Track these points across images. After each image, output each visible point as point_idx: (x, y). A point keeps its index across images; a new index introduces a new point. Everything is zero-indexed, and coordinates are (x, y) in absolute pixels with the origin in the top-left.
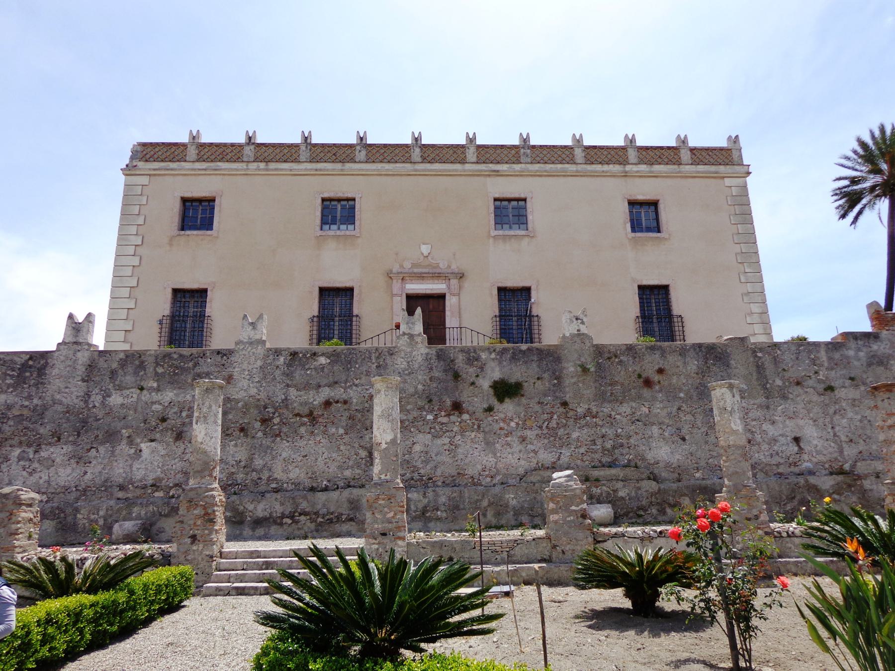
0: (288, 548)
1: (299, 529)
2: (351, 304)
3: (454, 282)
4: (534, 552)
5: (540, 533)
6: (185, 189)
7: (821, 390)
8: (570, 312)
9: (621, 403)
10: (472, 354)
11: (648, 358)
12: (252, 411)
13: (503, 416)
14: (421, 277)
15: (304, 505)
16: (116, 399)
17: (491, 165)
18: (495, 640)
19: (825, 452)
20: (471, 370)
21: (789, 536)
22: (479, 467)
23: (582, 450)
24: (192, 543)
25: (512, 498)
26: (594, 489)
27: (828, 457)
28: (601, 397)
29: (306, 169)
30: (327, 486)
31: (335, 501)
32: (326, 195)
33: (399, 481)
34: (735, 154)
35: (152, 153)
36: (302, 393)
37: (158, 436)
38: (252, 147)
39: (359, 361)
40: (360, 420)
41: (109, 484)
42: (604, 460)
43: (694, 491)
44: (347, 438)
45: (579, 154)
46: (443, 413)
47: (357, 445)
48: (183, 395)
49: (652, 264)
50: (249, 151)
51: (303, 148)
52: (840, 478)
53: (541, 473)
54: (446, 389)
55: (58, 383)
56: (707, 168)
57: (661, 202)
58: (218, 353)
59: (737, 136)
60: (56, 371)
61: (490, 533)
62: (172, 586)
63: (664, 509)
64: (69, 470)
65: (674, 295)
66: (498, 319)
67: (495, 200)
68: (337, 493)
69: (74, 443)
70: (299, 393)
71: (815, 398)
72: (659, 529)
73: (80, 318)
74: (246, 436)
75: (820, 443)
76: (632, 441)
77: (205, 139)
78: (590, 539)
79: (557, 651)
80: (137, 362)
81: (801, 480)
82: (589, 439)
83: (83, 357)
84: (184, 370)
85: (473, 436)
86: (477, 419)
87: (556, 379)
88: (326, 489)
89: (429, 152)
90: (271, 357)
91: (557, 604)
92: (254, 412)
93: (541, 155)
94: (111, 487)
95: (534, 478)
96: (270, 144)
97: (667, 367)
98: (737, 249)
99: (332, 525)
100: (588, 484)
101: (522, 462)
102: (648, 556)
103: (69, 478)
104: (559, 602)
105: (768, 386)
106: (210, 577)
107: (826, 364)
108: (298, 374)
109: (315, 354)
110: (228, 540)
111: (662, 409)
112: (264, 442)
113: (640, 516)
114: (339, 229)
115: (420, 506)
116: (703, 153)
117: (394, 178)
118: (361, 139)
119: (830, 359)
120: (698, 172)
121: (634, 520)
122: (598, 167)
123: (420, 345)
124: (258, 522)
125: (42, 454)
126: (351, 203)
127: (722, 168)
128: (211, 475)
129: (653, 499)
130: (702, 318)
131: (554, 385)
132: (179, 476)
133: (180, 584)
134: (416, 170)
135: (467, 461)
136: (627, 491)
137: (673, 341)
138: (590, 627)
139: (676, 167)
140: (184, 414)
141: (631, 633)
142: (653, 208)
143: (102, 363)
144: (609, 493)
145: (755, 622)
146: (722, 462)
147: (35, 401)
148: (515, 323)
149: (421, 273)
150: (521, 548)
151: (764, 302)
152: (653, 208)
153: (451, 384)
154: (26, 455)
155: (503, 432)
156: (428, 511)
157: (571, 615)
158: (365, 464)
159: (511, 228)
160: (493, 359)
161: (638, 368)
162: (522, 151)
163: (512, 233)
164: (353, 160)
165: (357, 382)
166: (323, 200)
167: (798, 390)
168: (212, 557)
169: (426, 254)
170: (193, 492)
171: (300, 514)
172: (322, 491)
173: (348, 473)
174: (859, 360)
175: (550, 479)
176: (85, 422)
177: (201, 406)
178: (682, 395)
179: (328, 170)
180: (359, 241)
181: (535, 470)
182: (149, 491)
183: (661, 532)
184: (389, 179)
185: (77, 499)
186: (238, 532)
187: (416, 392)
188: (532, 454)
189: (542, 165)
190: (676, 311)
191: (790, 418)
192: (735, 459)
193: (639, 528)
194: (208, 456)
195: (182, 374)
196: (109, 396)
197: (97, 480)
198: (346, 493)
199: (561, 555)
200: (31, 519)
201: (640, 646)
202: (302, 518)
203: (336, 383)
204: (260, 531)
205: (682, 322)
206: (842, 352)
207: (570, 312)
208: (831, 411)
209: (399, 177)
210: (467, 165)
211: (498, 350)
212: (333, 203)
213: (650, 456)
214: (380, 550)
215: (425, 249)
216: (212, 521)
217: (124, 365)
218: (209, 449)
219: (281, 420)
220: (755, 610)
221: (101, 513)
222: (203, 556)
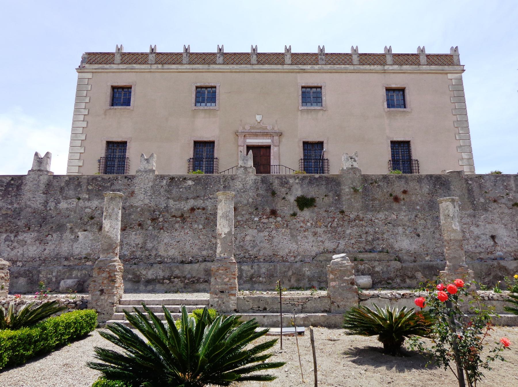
0: (162, 299)
1: (174, 286)
2: (213, 151)
3: (276, 138)
4: (319, 305)
5: (324, 293)
6: (114, 80)
7: (511, 206)
8: (347, 154)
9: (378, 212)
10: (283, 180)
11: (397, 184)
12: (146, 213)
13: (302, 219)
14: (256, 135)
15: (177, 272)
16: (63, 205)
17: (300, 66)
18: (286, 370)
19: (512, 245)
20: (283, 190)
21: (489, 299)
22: (287, 251)
23: (353, 241)
24: (101, 294)
25: (307, 271)
26: (360, 266)
27: (513, 250)
28: (366, 208)
29: (186, 69)
30: (191, 261)
31: (195, 270)
32: (198, 85)
33: (233, 258)
34: (455, 59)
35: (94, 59)
36: (177, 203)
37: (88, 228)
38: (154, 55)
39: (212, 184)
40: (211, 221)
41: (59, 257)
42: (367, 248)
43: (424, 268)
44: (204, 231)
45: (355, 58)
46: (265, 217)
47: (210, 236)
50: (152, 57)
51: (185, 55)
53: (326, 255)
54: (267, 202)
55: (29, 195)
57: (406, 89)
60: (28, 187)
61: (292, 292)
62: (80, 323)
63: (405, 279)
64: (35, 248)
65: (413, 147)
66: (303, 161)
67: (303, 87)
68: (198, 265)
69: (38, 231)
71: (506, 211)
72: (402, 292)
73: (42, 155)
74: (142, 228)
75: (508, 240)
76: (385, 236)
78: (356, 299)
79: (329, 382)
80: (76, 183)
81: (495, 263)
83: (44, 179)
85: (283, 231)
86: (286, 221)
88: (191, 262)
89: (261, 58)
91: (333, 342)
92: (147, 214)
93: (331, 60)
94: (60, 258)
95: (321, 258)
96: (164, 53)
97: (409, 190)
98: (455, 118)
99: (194, 284)
100: (356, 263)
101: (314, 248)
102: (396, 314)
103: (35, 252)
104: (334, 340)
105: (475, 202)
106: (111, 316)
107: (514, 189)
109: (185, 179)
110: (125, 292)
111: (405, 216)
113: (389, 283)
114: (206, 105)
115: (249, 274)
116: (435, 58)
117: (240, 73)
118: (220, 50)
122: (367, 67)
123: (251, 174)
124: (149, 282)
125: (19, 238)
126: (213, 89)
127: (446, 67)
128: (113, 252)
129: (398, 273)
130: (430, 160)
131: (336, 200)
133: (87, 321)
134: (253, 69)
135: (279, 247)
136: (381, 267)
137: (411, 173)
138: (354, 362)
139: (417, 66)
141: (383, 368)
142: (401, 93)
143: (55, 183)
144: (369, 269)
145: (480, 369)
146: (445, 250)
147: (15, 205)
148: (313, 164)
149: (256, 133)
150: (311, 303)
151: (471, 152)
152: (401, 93)
153: (270, 198)
154: (9, 238)
155: (302, 229)
156: (254, 278)
157: (341, 352)
159: (312, 105)
160: (297, 183)
161: (390, 190)
162: (320, 57)
163: (312, 108)
164: (215, 63)
165: (211, 196)
166: (197, 87)
167: (495, 205)
168: (113, 304)
169: (259, 121)
170: (102, 263)
171: (175, 278)
172: (188, 263)
173: (204, 253)
175: (331, 259)
176: (44, 219)
177: (108, 208)
178: (418, 207)
179: (200, 69)
180: (218, 112)
181: (322, 253)
182: (83, 261)
183: (403, 295)
185: (40, 265)
186: (136, 288)
187: (248, 203)
188: (321, 243)
189: (332, 66)
190: (414, 157)
191: (489, 223)
192: (455, 248)
193: (389, 291)
194: (112, 240)
195: (103, 190)
196: (59, 203)
197: (52, 254)
198: (203, 265)
199: (337, 308)
200: (3, 277)
201: (390, 380)
202: (176, 280)
203: (198, 197)
204: (150, 287)
205: (418, 164)
207: (347, 154)
209: (243, 74)
210: (285, 66)
211: (300, 177)
212: (203, 89)
213: (396, 246)
214: (220, 302)
215: (259, 118)
216: (113, 281)
218: (112, 236)
219: (164, 219)
220: (481, 361)
221: (54, 274)
222: (108, 303)
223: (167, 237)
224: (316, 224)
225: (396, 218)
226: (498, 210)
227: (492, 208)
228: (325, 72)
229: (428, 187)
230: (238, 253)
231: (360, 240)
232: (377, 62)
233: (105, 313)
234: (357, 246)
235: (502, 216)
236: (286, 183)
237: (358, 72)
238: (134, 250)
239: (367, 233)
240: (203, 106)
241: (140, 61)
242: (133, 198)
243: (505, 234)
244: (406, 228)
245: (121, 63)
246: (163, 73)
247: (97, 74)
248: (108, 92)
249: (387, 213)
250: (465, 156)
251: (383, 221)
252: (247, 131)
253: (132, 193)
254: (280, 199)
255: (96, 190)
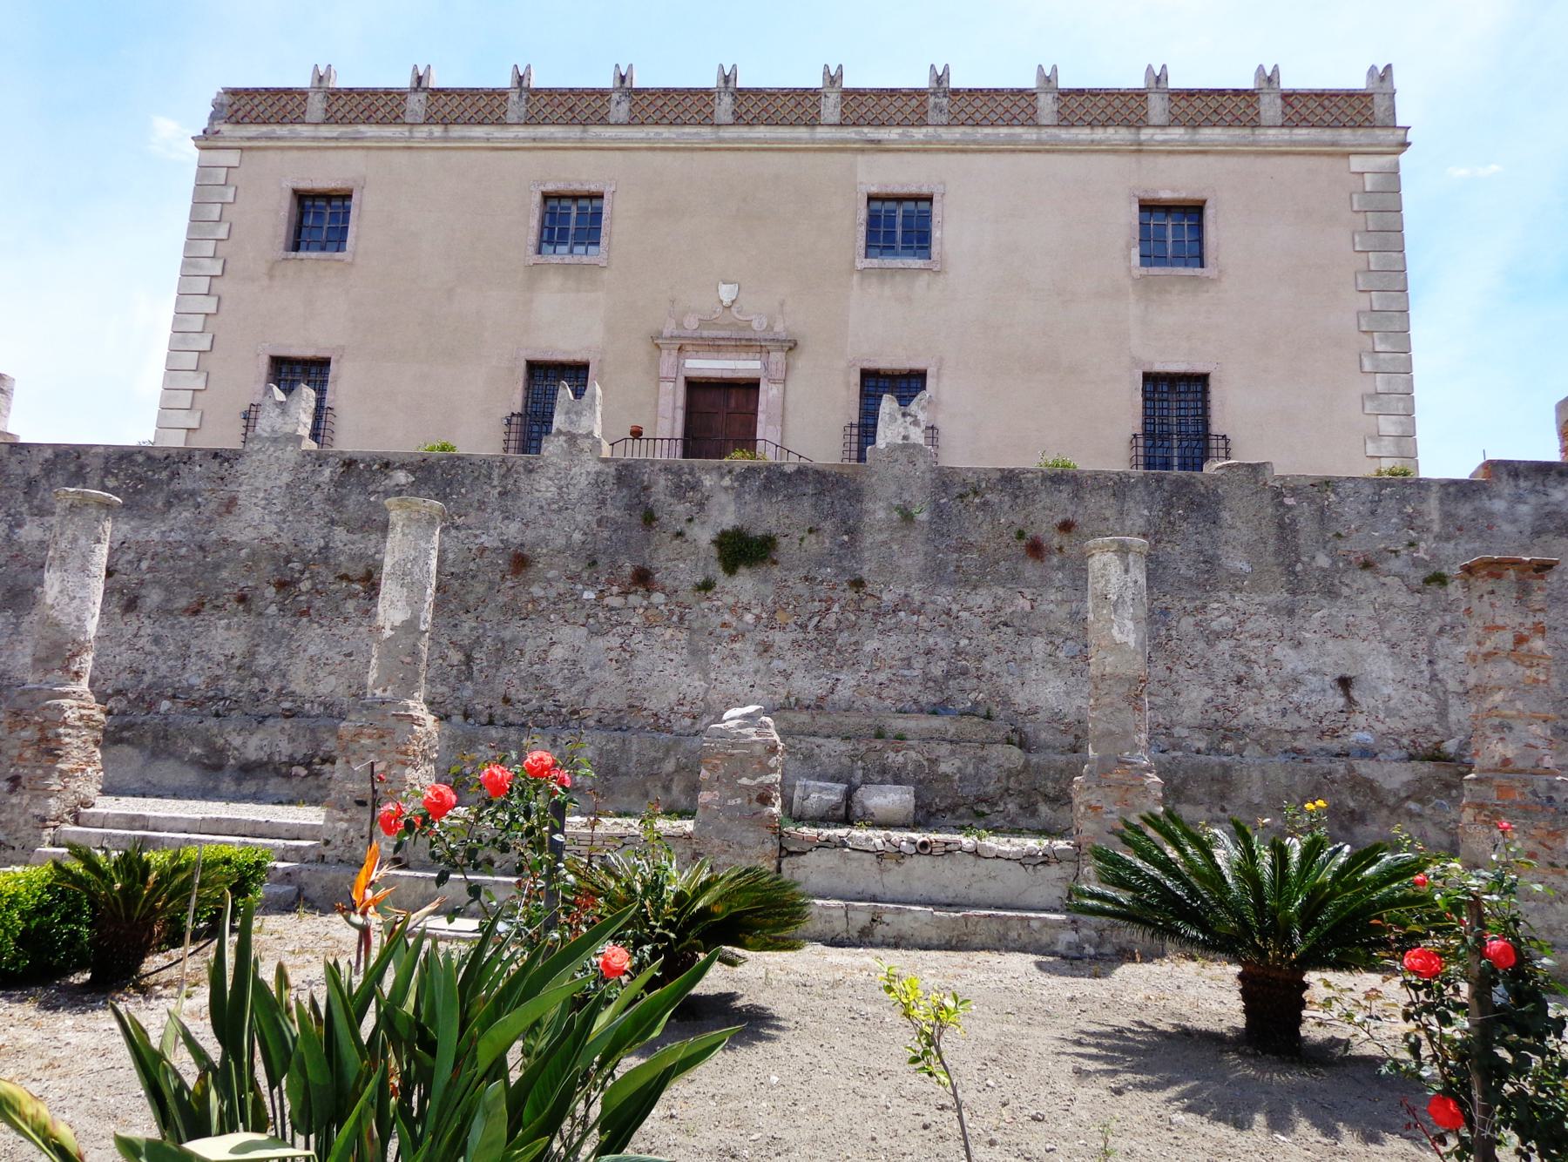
0: (199, 816)
3: (777, 357)
6: (302, 175)
7: (1417, 582)
9: (975, 588)
10: (685, 477)
11: (1044, 499)
12: (262, 565)
13: (730, 600)
14: (715, 346)
17: (866, 130)
19: (1406, 713)
20: (680, 508)
22: (673, 697)
23: (882, 677)
24: (11, 791)
26: (892, 755)
27: (1410, 726)
28: (935, 573)
29: (516, 138)
32: (550, 187)
34: (1380, 104)
35: (248, 108)
38: (422, 96)
39: (467, 482)
42: (923, 700)
45: (1046, 104)
46: (615, 589)
47: (444, 641)
48: (145, 531)
49: (1177, 328)
50: (416, 104)
51: (514, 97)
52: (1426, 768)
53: (789, 715)
56: (1314, 133)
58: (216, 455)
59: (1389, 67)
66: (855, 431)
67: (871, 198)
70: (351, 536)
71: (1402, 598)
72: (919, 837)
74: (248, 611)
77: (340, 82)
80: (72, 467)
81: (1340, 767)
82: (899, 655)
84: (153, 485)
85: (667, 636)
86: (678, 605)
87: (846, 533)
90: (309, 468)
92: (267, 567)
93: (970, 110)
96: (454, 90)
98: (1363, 302)
105: (1299, 567)
107: (1436, 528)
108: (354, 500)
109: (387, 465)
111: (1059, 604)
112: (278, 624)
113: (982, 815)
114: (571, 251)
116: (1312, 104)
118: (623, 79)
119: (1447, 516)
120: (1294, 143)
121: (966, 822)
122: (1083, 134)
123: (585, 457)
124: (248, 770)
127: (1346, 135)
128: (66, 669)
131: (842, 545)
132: (125, 675)
134: (721, 140)
135: (650, 683)
136: (958, 763)
139: (1247, 131)
140: (144, 565)
144: (921, 766)
149: (714, 339)
151: (1409, 414)
153: (638, 534)
155: (726, 632)
158: (457, 677)
160: (726, 489)
161: (1018, 519)
162: (932, 100)
164: (603, 121)
165: (459, 521)
166: (546, 197)
167: (1367, 578)
168: (44, 820)
169: (727, 301)
170: (26, 698)
174: (1515, 521)
179: (555, 140)
180: (606, 274)
183: (924, 845)
184: (669, 156)
186: (211, 784)
187: (568, 546)
189: (969, 130)
192: (1112, 704)
194: (64, 633)
195: (148, 492)
196: (20, 526)
204: (250, 786)
206: (1477, 503)
208: (1433, 627)
209: (687, 155)
210: (819, 129)
211: (738, 469)
212: (565, 203)
213: (1020, 698)
214: (352, 833)
215: (726, 293)
216: (49, 749)
217: (51, 471)
218: (65, 619)
219: (314, 586)
222: (28, 816)
223: (318, 640)
224: (771, 618)
225: (1028, 608)
226: (1375, 594)
227: (1355, 586)
228: (947, 151)
229: (1146, 512)
230: (522, 697)
231: (906, 672)
232: (1118, 118)
233: (17, 845)
234: (893, 693)
235: (1385, 614)
236: (693, 488)
237: (1053, 151)
238: (220, 672)
239: (928, 652)
240: (561, 255)
241: (380, 115)
242: (231, 517)
243: (1390, 674)
244: (1058, 641)
245: (327, 122)
246: (446, 153)
247: (254, 153)
248: (283, 207)
249: (1001, 591)
250: (1388, 426)
251: (986, 618)
252: (688, 333)
253: (230, 505)
254: (666, 537)
255: (126, 491)
